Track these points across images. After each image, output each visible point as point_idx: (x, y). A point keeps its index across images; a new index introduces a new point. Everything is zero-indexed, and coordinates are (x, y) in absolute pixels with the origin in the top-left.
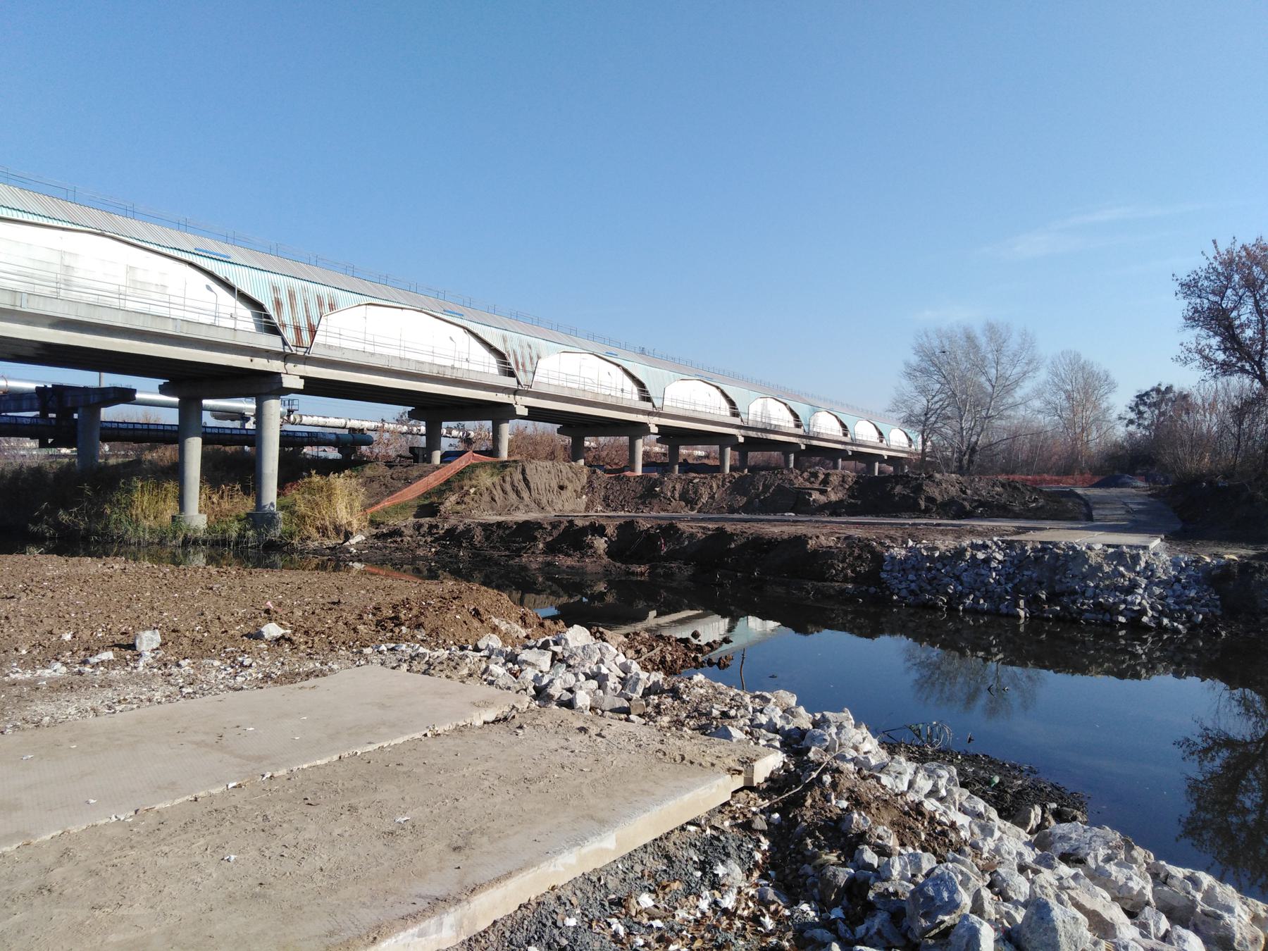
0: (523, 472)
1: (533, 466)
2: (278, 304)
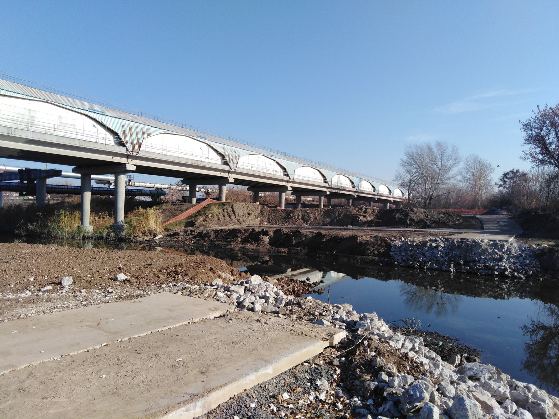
0: (232, 207)
1: (236, 205)
2: (124, 133)
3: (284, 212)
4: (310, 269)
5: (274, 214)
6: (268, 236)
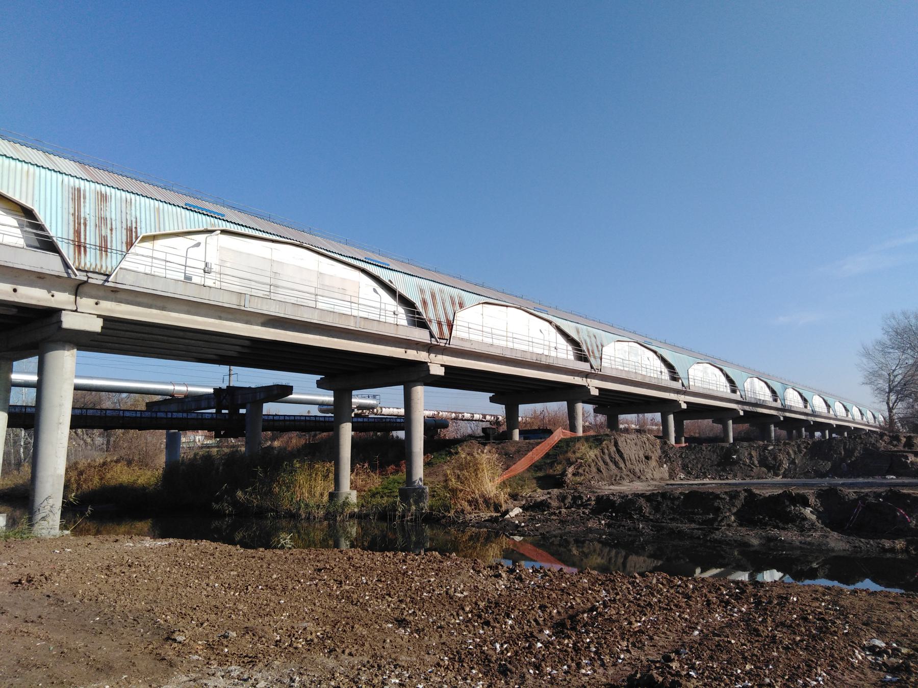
0: (616, 444)
1: (623, 439)
2: (425, 303)
3: (714, 452)
4: (722, 569)
5: (693, 457)
6: (809, 506)
